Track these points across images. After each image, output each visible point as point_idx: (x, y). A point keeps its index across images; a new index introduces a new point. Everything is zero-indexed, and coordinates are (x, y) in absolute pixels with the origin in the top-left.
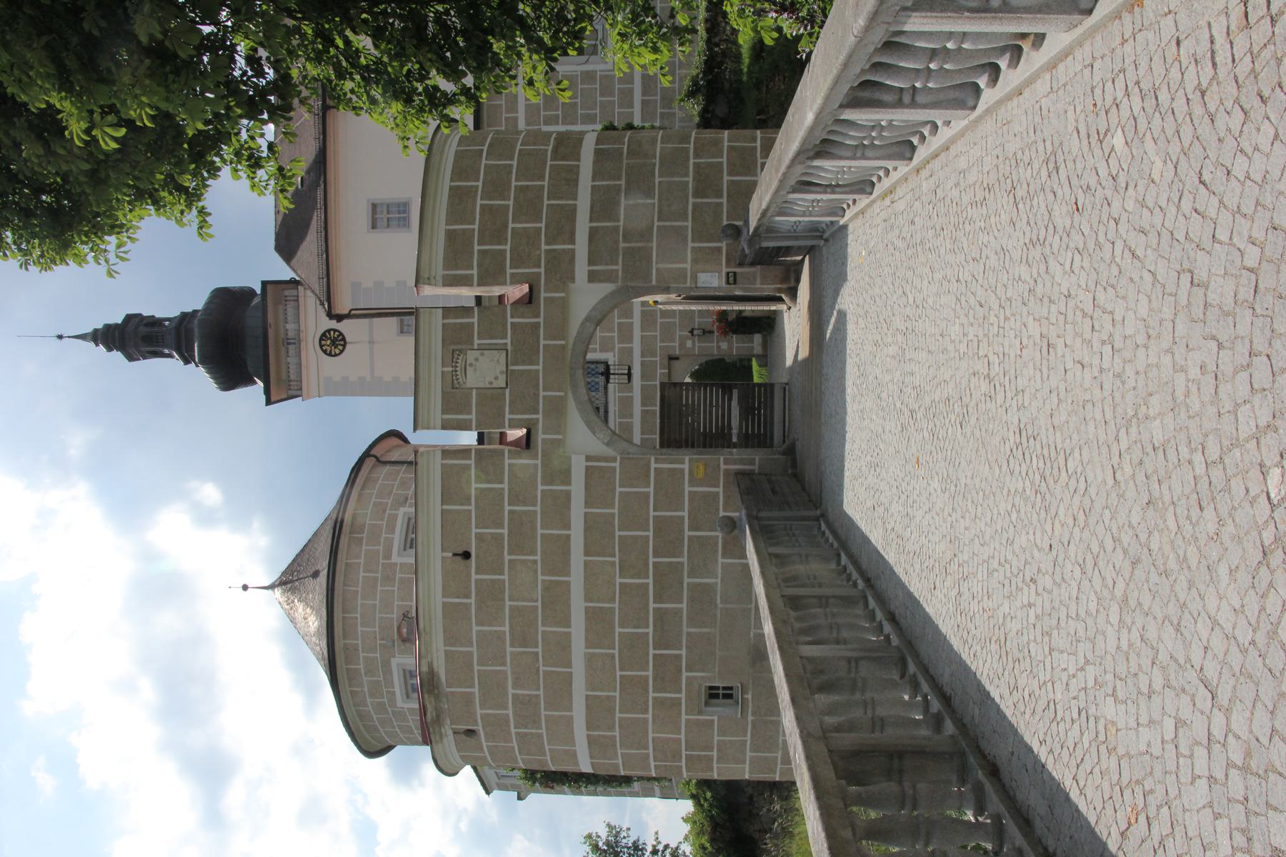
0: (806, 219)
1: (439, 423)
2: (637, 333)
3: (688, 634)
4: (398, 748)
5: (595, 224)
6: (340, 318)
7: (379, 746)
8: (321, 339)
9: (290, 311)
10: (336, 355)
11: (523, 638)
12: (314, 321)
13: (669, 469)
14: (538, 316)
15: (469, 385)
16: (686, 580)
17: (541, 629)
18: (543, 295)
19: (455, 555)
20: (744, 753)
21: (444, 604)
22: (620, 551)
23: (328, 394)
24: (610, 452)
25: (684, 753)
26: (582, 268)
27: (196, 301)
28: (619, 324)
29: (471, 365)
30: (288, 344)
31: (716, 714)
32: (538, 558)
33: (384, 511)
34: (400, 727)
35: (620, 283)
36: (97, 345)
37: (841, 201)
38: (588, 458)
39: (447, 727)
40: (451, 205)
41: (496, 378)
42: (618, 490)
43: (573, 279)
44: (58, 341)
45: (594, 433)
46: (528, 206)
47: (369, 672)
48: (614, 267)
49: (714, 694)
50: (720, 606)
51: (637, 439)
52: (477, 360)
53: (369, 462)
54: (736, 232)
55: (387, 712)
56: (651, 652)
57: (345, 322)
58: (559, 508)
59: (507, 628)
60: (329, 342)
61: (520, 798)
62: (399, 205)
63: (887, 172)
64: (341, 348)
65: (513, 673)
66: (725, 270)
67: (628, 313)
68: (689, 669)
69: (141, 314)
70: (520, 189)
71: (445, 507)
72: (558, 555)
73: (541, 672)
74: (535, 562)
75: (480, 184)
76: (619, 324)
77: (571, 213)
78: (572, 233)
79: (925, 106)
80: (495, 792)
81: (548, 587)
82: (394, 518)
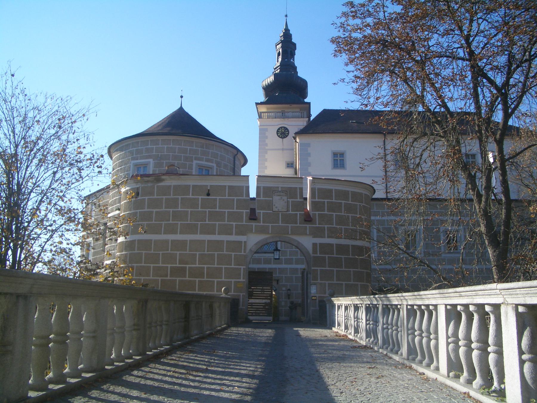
1: (259, 185)
2: (289, 266)
5: (335, 245)
7: (112, 151)
8: (284, 127)
10: (277, 134)
13: (241, 273)
14: (300, 224)
16: (197, 280)
17: (179, 222)
18: (308, 226)
19: (209, 190)
21: (190, 185)
22: (209, 254)
24: (248, 251)
26: (318, 241)
29: (281, 198)
30: (283, 113)
35: (312, 255)
38: (245, 242)
39: (140, 185)
41: (276, 207)
42: (233, 254)
43: (315, 237)
48: (318, 253)
52: (283, 200)
58: (226, 230)
60: (283, 131)
62: (343, 164)
64: (281, 136)
66: (317, 295)
69: (296, 49)
70: (139, 249)
71: (227, 187)
73: (162, 222)
74: (206, 221)
75: (350, 202)
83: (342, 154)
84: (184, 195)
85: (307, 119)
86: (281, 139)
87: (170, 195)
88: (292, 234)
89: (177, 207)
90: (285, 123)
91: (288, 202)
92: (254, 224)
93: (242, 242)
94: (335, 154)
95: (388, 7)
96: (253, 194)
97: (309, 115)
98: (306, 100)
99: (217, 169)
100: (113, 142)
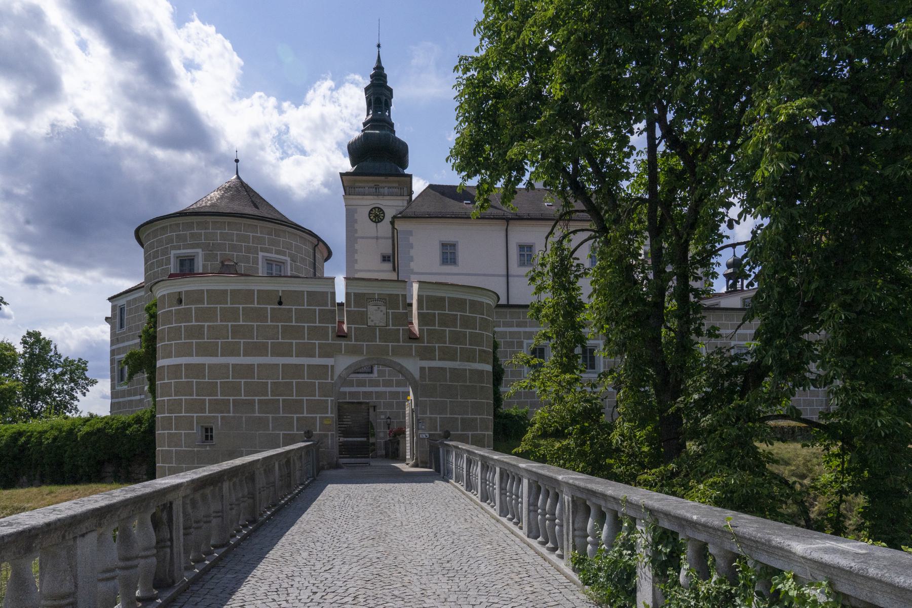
0: (454, 467)
1: (349, 291)
2: (388, 389)
3: (242, 417)
4: (142, 250)
6: (392, 223)
7: (143, 238)
8: (379, 208)
9: (395, 190)
10: (370, 217)
11: (236, 331)
12: (391, 206)
14: (403, 342)
15: (369, 307)
17: (242, 341)
20: (175, 446)
23: (347, 210)
24: (336, 377)
25: (173, 415)
26: (427, 364)
27: (401, 132)
28: (392, 380)
31: (196, 432)
32: (280, 340)
33: (287, 249)
34: (157, 251)
36: (374, 69)
37: (463, 481)
38: (332, 367)
40: (457, 299)
41: (372, 321)
42: (317, 381)
44: (376, 44)
45: (345, 369)
46: (457, 338)
47: (193, 236)
49: (208, 433)
50: (257, 433)
51: (343, 389)
52: (381, 311)
53: (315, 241)
54: (447, 435)
55: (167, 244)
56: (231, 398)
57: (390, 226)
59: (241, 323)
61: (107, 319)
62: (455, 259)
63: (475, 495)
65: (216, 325)
67: (399, 384)
68: (222, 418)
69: (392, 97)
72: (279, 351)
74: (278, 339)
76: (392, 380)
77: (453, 359)
78: (444, 359)
79: (500, 498)
80: (110, 304)
81: (265, 345)
82: (284, 254)
83: (453, 246)
84: (246, 304)
85: (408, 198)
86: (375, 224)
87: (227, 304)
88: (393, 354)
89: (237, 320)
90: (379, 202)
91: (387, 314)
92: (343, 343)
93: (328, 366)
94: (444, 245)
95: (78, 400)
96: (340, 297)
97: (411, 193)
98: (406, 171)
99: (291, 264)
100: (145, 221)
